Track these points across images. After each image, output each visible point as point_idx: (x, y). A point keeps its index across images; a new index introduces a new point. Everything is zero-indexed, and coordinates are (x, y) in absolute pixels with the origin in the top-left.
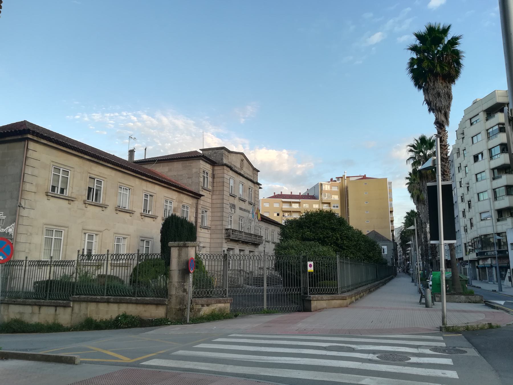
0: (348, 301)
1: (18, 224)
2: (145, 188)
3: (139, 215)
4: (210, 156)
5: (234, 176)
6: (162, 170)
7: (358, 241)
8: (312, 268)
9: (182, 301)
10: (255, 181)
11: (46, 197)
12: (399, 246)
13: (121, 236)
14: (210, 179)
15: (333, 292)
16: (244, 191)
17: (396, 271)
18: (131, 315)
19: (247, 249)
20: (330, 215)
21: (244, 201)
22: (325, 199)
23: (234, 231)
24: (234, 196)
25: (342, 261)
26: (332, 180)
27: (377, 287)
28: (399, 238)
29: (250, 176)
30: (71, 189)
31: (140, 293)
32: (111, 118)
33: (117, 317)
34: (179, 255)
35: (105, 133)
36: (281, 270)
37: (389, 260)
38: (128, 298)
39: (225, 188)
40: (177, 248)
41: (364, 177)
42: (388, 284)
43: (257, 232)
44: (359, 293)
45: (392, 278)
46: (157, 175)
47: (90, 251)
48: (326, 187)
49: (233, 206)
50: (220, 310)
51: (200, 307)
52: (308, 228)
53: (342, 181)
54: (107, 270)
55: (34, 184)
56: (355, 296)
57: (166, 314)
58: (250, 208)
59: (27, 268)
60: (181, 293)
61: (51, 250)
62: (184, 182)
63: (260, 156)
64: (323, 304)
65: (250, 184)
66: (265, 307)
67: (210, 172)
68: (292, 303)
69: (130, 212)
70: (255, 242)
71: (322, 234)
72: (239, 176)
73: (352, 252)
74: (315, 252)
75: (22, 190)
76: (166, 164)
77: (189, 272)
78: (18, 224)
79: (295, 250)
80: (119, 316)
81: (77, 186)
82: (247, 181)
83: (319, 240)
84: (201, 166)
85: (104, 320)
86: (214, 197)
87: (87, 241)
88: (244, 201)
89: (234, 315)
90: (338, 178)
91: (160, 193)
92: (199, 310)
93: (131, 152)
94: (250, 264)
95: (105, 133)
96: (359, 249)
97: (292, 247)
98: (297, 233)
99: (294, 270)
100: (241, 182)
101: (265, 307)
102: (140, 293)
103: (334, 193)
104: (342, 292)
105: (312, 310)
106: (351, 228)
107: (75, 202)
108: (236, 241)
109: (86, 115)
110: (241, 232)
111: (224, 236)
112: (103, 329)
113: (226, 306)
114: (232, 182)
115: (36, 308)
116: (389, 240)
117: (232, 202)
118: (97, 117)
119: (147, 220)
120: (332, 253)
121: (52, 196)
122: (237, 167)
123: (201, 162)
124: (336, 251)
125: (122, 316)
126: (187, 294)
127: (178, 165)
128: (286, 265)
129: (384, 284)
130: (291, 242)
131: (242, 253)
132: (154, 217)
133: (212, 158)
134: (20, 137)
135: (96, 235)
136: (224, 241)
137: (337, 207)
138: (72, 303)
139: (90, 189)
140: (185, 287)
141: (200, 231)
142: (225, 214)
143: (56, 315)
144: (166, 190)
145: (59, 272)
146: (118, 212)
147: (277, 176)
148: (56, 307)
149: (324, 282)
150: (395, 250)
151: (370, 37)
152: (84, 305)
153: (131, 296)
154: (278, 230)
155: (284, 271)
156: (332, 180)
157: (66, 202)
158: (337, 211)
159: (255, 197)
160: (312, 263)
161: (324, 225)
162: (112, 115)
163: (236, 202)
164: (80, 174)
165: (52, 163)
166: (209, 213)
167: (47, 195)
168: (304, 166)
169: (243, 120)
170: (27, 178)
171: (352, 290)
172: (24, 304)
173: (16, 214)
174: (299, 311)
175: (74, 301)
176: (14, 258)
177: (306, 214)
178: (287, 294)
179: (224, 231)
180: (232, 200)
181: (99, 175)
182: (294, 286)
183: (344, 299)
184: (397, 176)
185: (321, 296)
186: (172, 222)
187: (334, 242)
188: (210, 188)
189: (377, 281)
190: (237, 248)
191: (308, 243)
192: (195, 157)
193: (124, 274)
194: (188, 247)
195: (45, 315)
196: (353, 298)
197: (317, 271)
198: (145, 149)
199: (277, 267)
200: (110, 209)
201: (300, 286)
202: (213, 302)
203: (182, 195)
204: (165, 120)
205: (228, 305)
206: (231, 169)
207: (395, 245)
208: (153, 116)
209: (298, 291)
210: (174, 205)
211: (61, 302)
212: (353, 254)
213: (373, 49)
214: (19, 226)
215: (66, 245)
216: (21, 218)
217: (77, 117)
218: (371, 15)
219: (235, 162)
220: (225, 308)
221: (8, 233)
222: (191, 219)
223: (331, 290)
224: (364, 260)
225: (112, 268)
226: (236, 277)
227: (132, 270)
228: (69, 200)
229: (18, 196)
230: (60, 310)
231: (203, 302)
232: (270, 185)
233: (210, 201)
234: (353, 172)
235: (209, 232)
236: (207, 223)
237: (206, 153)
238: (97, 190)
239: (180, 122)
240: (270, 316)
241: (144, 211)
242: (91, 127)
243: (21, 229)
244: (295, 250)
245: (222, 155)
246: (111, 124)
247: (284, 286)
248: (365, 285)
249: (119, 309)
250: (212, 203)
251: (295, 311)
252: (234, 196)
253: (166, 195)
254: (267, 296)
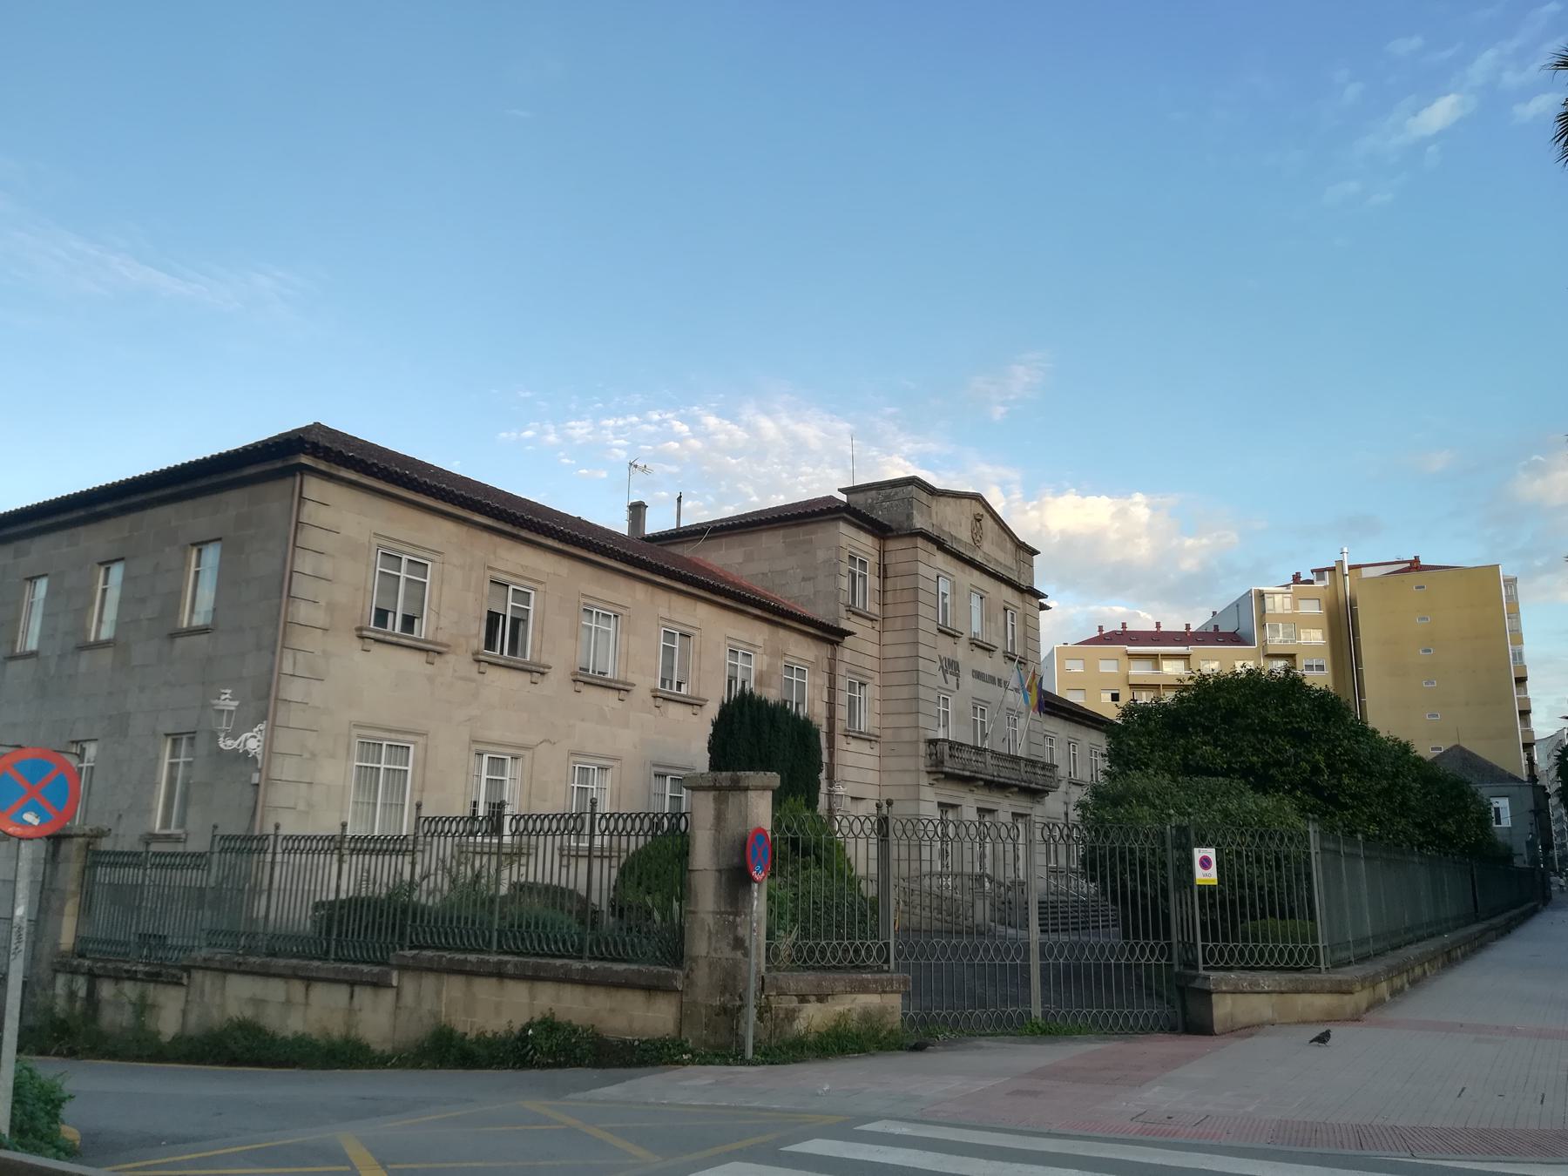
0: (1362, 998)
1: (273, 725)
2: (663, 612)
3: (649, 695)
4: (872, 507)
5: (951, 570)
6: (723, 559)
7: (1396, 775)
8: (1213, 870)
9: (729, 981)
10: (1024, 583)
11: (357, 644)
12: (1553, 801)
13: (592, 764)
14: (873, 582)
15: (1297, 962)
16: (987, 617)
17: (1546, 885)
18: (569, 1023)
19: (1006, 807)
20: (1291, 686)
21: (988, 649)
22: (1277, 640)
23: (955, 746)
24: (953, 635)
25: (1332, 846)
26: (1296, 578)
27: (1476, 945)
28: (1553, 773)
29: (1011, 571)
30: (433, 617)
31: (598, 946)
32: (618, 431)
33: (524, 1030)
34: (719, 818)
35: (604, 475)
36: (1103, 878)
37: (1520, 847)
38: (558, 962)
39: (922, 610)
40: (711, 794)
41: (1415, 566)
42: (1517, 933)
43: (1035, 750)
44: (1400, 970)
45: (1534, 912)
46: (710, 573)
47: (497, 810)
48: (1279, 604)
49: (951, 667)
50: (866, 1016)
51: (794, 1003)
52: (1207, 730)
53: (1334, 580)
54: (543, 867)
55: (323, 603)
56: (1390, 979)
57: (680, 1024)
58: (1010, 673)
59: (279, 858)
60: (727, 952)
61: (375, 805)
62: (791, 594)
63: (1056, 516)
64: (1260, 1006)
65: (1007, 593)
66: (1037, 1010)
67: (872, 561)
68: (1149, 995)
69: (621, 688)
70: (1030, 782)
71: (1256, 751)
72: (967, 569)
73: (1373, 818)
74: (1226, 814)
75: (285, 623)
76: (736, 539)
77: (749, 880)
78: (273, 725)
79: (1154, 806)
80: (529, 1025)
81: (453, 609)
82: (998, 583)
83: (1246, 772)
84: (844, 542)
85: (489, 1035)
86: (888, 637)
87: (485, 776)
88: (988, 649)
89: (914, 1038)
90: (1320, 572)
91: (716, 629)
92: (791, 1015)
93: (637, 510)
94: (1016, 858)
95: (604, 475)
96: (1403, 804)
97: (1143, 798)
98: (1165, 748)
99: (1153, 876)
100: (974, 589)
101: (1037, 1010)
102: (598, 946)
103: (1309, 622)
104: (1338, 965)
105: (1216, 1029)
106: (1363, 732)
107: (448, 657)
108: (967, 781)
109: (550, 427)
110: (979, 751)
111: (922, 763)
112: (480, 1067)
113: (883, 1003)
114: (944, 586)
115: (298, 987)
116: (1516, 779)
117: (949, 655)
118: (580, 429)
119: (674, 710)
120: (1293, 818)
121: (377, 640)
122: (959, 541)
123: (844, 528)
124: (1303, 811)
125: (540, 1023)
126: (746, 954)
127: (771, 541)
128: (1122, 859)
129: (1506, 930)
130: (1138, 780)
131: (950, 816)
132: (695, 703)
133: (879, 515)
134: (279, 464)
135: (515, 758)
136: (925, 780)
137: (1321, 668)
138: (395, 974)
139: (493, 619)
140: (741, 932)
141: (845, 747)
142: (922, 692)
143: (351, 1011)
144: (729, 617)
145: (385, 873)
146: (579, 686)
147: (1118, 579)
148: (352, 984)
149: (1261, 921)
150: (1540, 811)
151: (1415, 114)
152: (429, 981)
153: (570, 957)
154: (1100, 741)
155: (1114, 880)
156: (1296, 578)
157: (420, 658)
158: (1319, 679)
159: (1026, 636)
160: (1211, 853)
161: (1264, 720)
162: (621, 422)
163: (961, 652)
164: (459, 573)
165: (375, 541)
166: (871, 691)
167: (362, 637)
168: (1205, 541)
169: (1002, 410)
170: (301, 587)
171: (1379, 954)
172: (265, 973)
173: (268, 696)
174: (1173, 1030)
175: (403, 968)
176: (261, 828)
177: (1198, 684)
178: (1118, 966)
179: (922, 747)
180: (945, 647)
181: (520, 571)
182: (1146, 936)
183: (1341, 990)
184: (1538, 563)
185: (1249, 975)
186: (742, 713)
187: (1305, 782)
188: (873, 608)
189: (1477, 920)
190: (969, 803)
191: (1202, 782)
192: (822, 513)
193: (597, 882)
194: (747, 789)
195: (318, 1010)
196: (1383, 988)
197: (1231, 880)
198: (679, 500)
199: (1091, 865)
200: (557, 679)
201: (1167, 935)
202: (840, 987)
203: (782, 633)
204: (767, 426)
205: (895, 1001)
206: (940, 545)
207: (1541, 794)
208: (734, 419)
209: (1162, 955)
210: (758, 663)
211: (365, 968)
212: (1380, 823)
213: (1432, 149)
214: (279, 732)
215: (422, 791)
216: (282, 708)
217: (529, 434)
218: (1416, 42)
219: (955, 523)
220: (883, 1011)
221: (246, 752)
222: (813, 707)
223: (1291, 953)
224: (1420, 846)
225: (565, 862)
226: (968, 898)
227: (614, 872)
228: (427, 651)
229: (276, 641)
230: (364, 996)
231: (804, 988)
232: (1092, 608)
233: (873, 650)
234: (1377, 550)
235: (876, 751)
236: (867, 721)
237: (860, 501)
238: (516, 623)
239: (810, 432)
240: (1047, 1048)
241: (663, 685)
242: (567, 461)
243: (284, 742)
244: (1154, 806)
245: (909, 502)
246: (619, 447)
247: (1126, 936)
248: (1432, 936)
249: (533, 998)
250: (882, 659)
251: (1161, 1030)
252: (953, 635)
253: (733, 633)
254: (1044, 969)
